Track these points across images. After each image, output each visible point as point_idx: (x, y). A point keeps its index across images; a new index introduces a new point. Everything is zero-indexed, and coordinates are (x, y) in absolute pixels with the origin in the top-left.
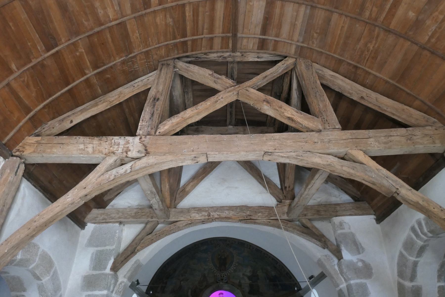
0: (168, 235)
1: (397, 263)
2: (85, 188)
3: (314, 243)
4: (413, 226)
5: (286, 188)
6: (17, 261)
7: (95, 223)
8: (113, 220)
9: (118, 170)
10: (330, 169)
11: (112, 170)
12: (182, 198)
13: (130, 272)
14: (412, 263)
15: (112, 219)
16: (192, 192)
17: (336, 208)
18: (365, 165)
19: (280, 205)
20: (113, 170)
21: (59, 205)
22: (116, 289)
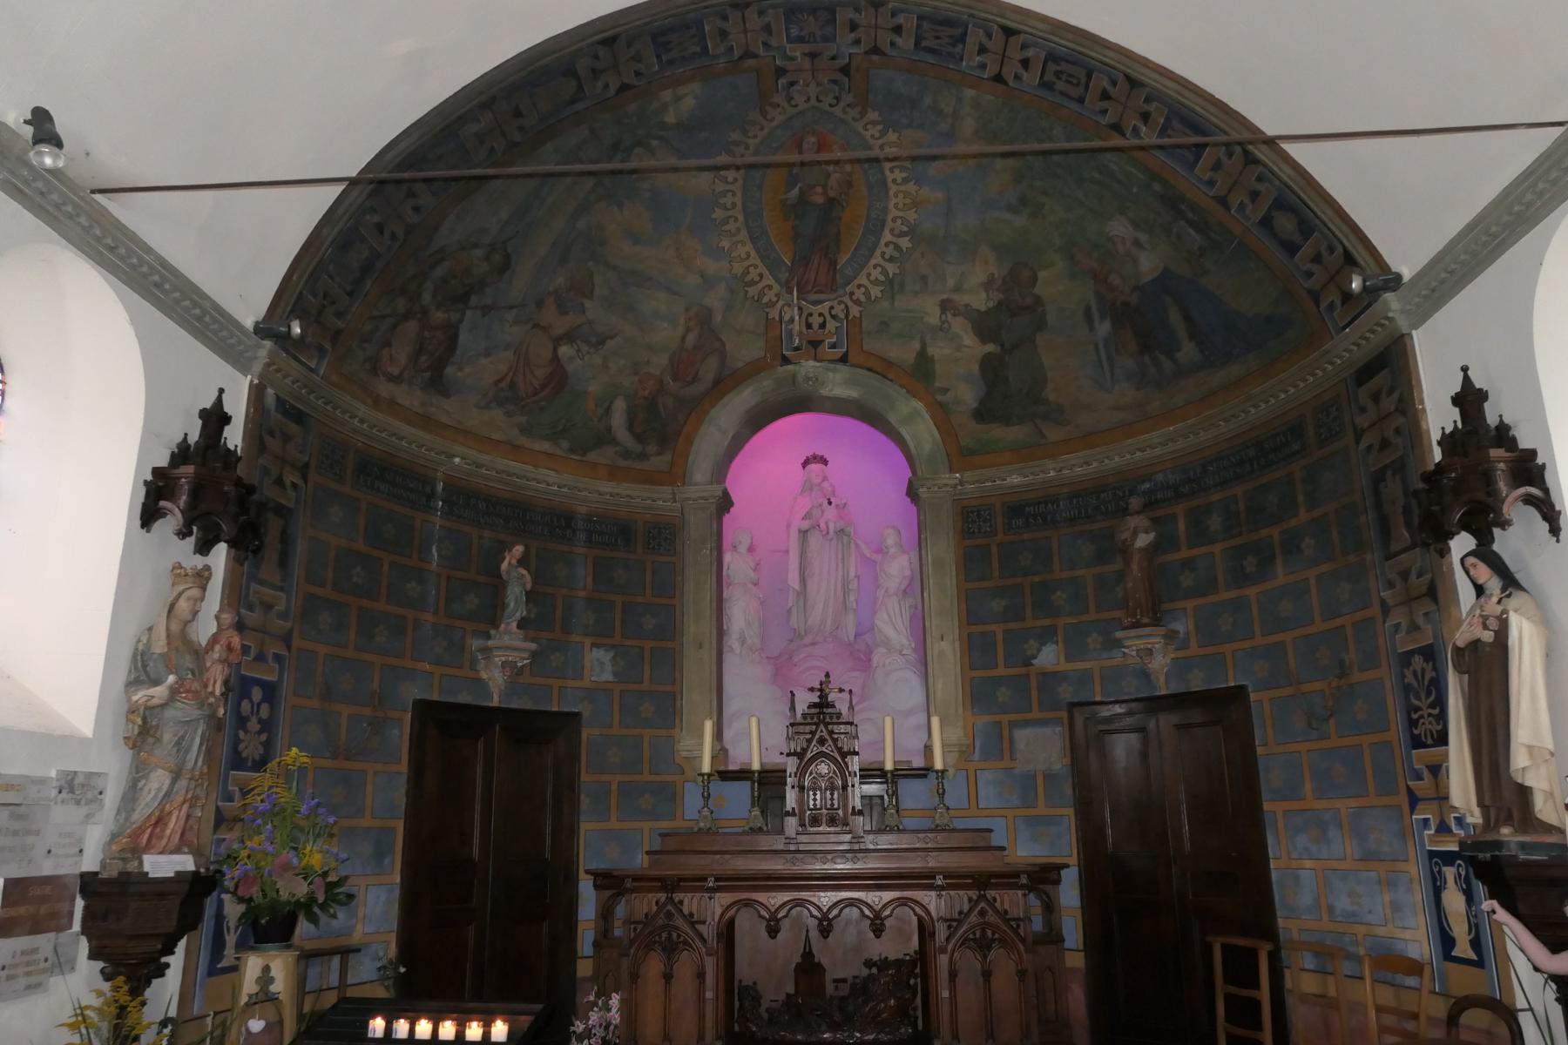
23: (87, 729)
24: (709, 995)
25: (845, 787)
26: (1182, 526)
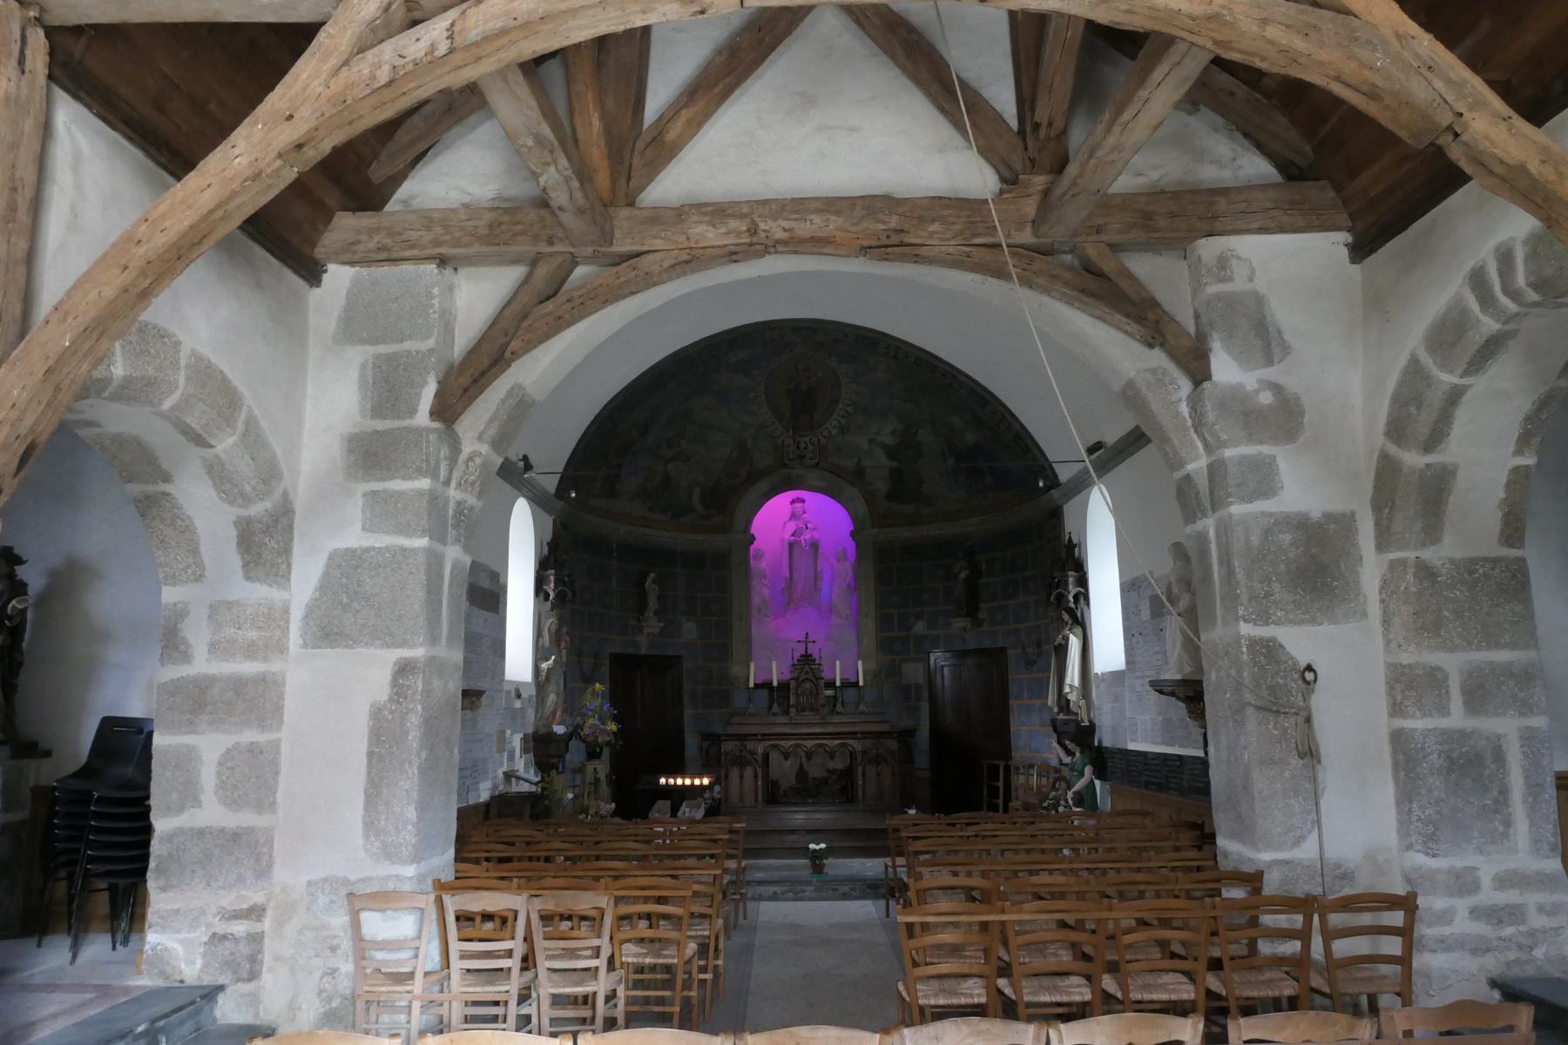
0: (611, 303)
1: (1393, 395)
2: (291, 116)
3: (1119, 328)
4: (1481, 267)
5: (1037, 126)
6: (115, 384)
7: (352, 263)
8: (415, 252)
9: (400, 43)
10: (1213, 34)
11: (379, 47)
12: (655, 167)
13: (496, 424)
14: (1444, 393)
15: (412, 247)
16: (688, 146)
17: (1212, 203)
18: (1356, 16)
19: (1010, 191)
20: (384, 44)
21: (208, 182)
22: (456, 475)
23: (530, 680)
24: (759, 783)
25: (817, 694)
26: (984, 567)
